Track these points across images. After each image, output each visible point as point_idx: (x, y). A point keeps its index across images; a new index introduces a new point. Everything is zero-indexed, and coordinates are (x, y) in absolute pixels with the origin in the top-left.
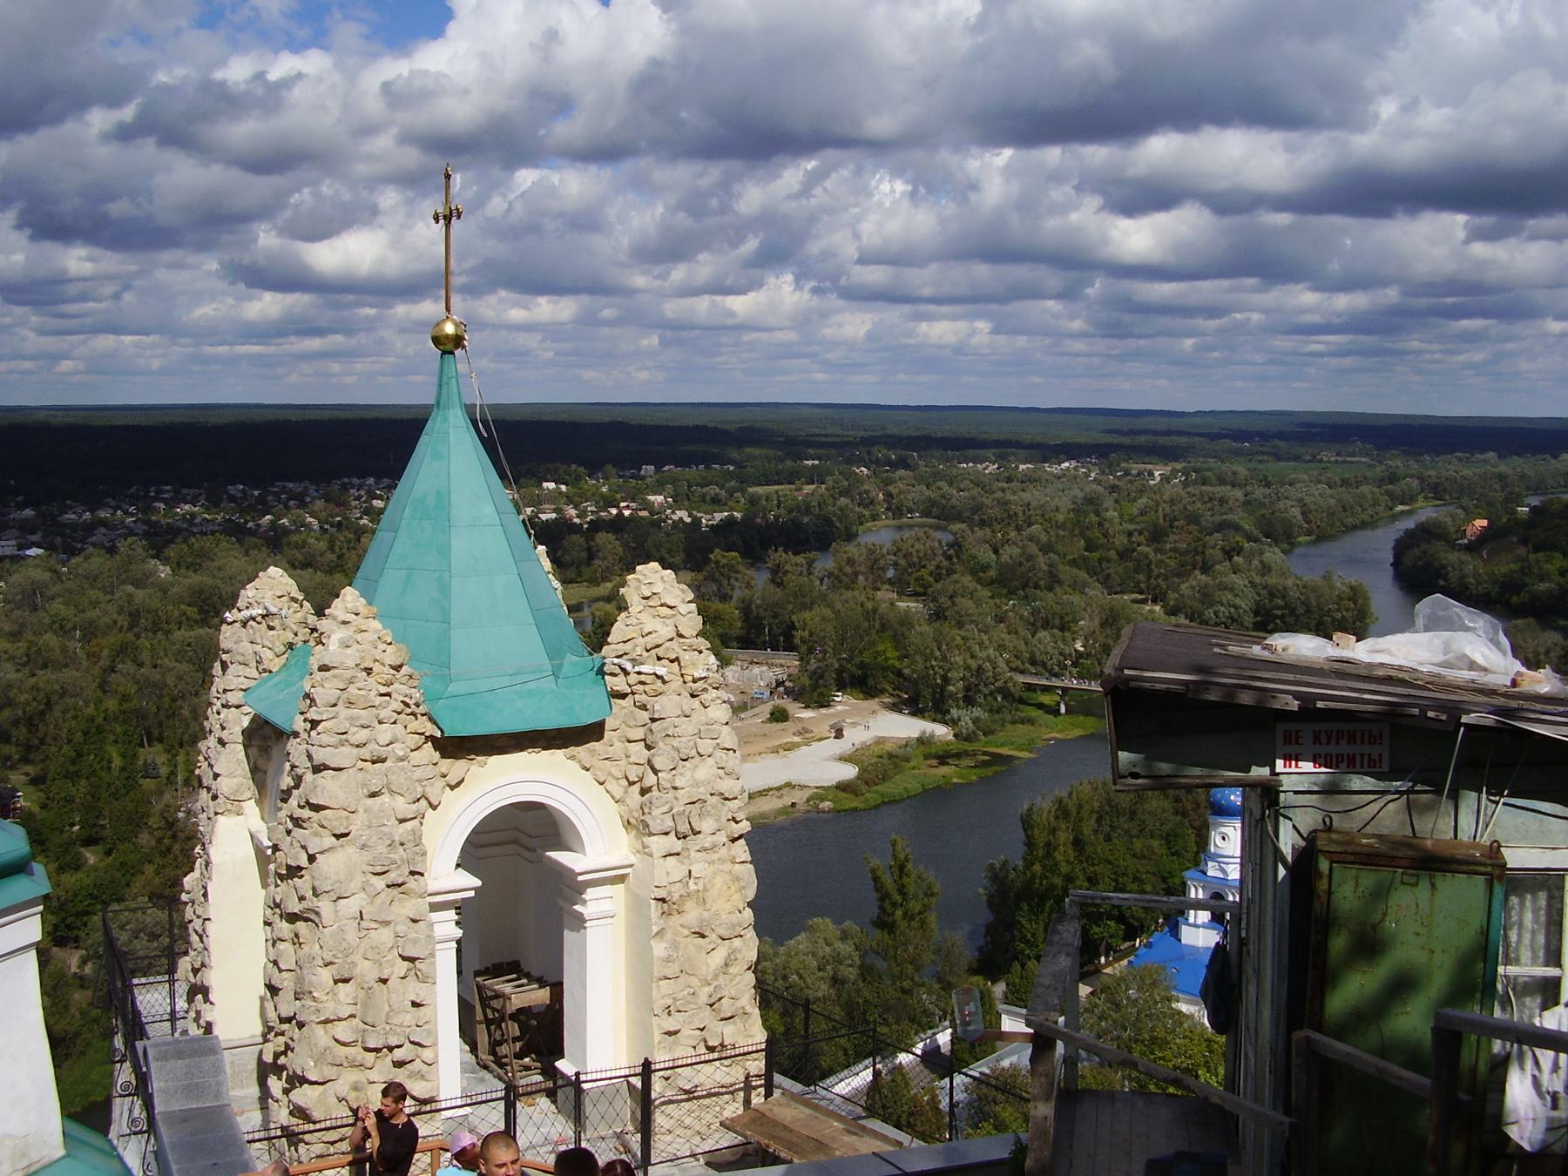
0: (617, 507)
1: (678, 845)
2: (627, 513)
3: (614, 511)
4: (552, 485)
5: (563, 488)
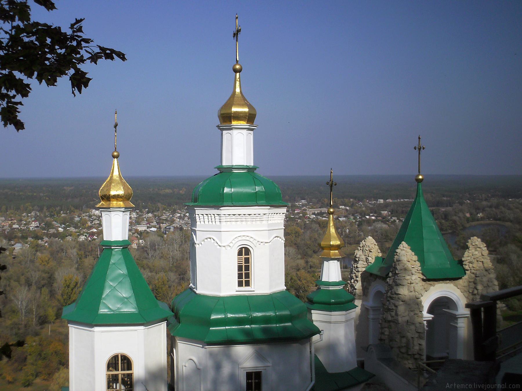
0: (369, 215)
2: (24, 214)
3: (368, 217)
4: (343, 207)
5: (348, 208)
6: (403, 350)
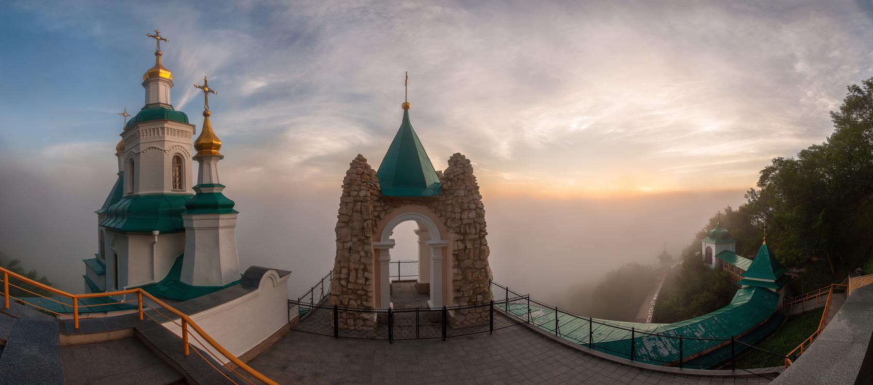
1: (462, 238)
6: (343, 283)
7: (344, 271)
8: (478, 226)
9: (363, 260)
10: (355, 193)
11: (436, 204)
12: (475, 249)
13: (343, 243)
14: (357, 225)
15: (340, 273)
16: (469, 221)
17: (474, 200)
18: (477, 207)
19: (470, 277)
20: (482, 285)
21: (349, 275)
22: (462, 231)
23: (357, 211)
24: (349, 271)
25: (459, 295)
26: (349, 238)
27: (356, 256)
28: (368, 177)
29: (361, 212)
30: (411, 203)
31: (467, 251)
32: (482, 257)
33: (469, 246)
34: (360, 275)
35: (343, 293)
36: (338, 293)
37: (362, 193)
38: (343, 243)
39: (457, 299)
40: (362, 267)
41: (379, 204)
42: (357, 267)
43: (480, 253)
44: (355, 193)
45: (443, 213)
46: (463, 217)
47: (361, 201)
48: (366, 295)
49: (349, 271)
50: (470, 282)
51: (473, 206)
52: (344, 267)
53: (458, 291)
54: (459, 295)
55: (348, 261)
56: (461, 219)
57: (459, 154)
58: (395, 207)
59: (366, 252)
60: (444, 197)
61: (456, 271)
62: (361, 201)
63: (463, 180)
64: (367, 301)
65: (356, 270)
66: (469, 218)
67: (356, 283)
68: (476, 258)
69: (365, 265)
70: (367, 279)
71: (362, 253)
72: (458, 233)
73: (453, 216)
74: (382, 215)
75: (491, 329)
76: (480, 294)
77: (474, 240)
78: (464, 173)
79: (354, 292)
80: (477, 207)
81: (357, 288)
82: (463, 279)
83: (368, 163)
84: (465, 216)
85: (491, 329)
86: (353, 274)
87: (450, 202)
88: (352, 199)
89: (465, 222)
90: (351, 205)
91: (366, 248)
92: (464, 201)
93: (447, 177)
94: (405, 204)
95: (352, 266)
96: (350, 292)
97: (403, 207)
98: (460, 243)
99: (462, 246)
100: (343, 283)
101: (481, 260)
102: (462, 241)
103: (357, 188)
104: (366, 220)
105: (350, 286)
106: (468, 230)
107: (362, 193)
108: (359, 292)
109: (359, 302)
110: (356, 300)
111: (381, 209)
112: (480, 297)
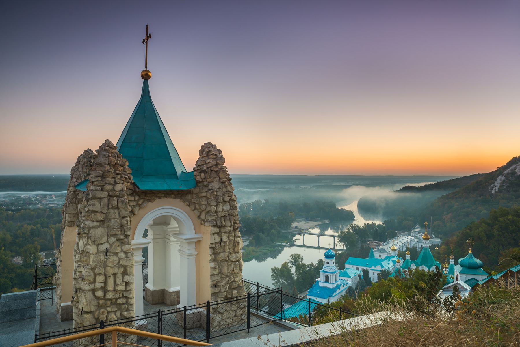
1: (217, 230)
6: (100, 294)
7: (100, 279)
8: (233, 219)
9: (123, 262)
10: (110, 187)
11: (189, 197)
12: (230, 241)
13: (98, 245)
14: (114, 223)
15: (95, 282)
16: (223, 214)
17: (228, 192)
18: (231, 200)
19: (225, 270)
20: (237, 279)
21: (105, 282)
22: (219, 224)
23: (113, 208)
24: (106, 277)
25: (217, 290)
26: (105, 239)
27: (114, 259)
28: (122, 168)
29: (118, 208)
30: (165, 197)
31: (223, 244)
32: (236, 249)
33: (225, 238)
34: (119, 281)
35: (99, 306)
36: (93, 309)
37: (119, 187)
38: (98, 245)
39: (214, 294)
40: (122, 270)
41: (133, 198)
42: (116, 270)
43: (235, 245)
44: (110, 187)
45: (197, 206)
46: (219, 210)
47: (116, 196)
48: (127, 303)
49: (106, 277)
50: (227, 276)
51: (227, 199)
52: (100, 274)
53: (215, 286)
54: (217, 290)
55: (105, 266)
56: (216, 212)
57: (210, 143)
58: (149, 201)
59: (126, 253)
60: (197, 190)
61: (213, 264)
62: (116, 196)
63: (216, 172)
64: (127, 310)
65: (115, 275)
66: (223, 211)
67: (115, 290)
68: (231, 250)
69: (125, 267)
70: (127, 284)
71: (122, 255)
72: (214, 226)
73: (208, 209)
74: (136, 210)
75: (249, 327)
76: (235, 288)
77: (229, 232)
78: (216, 165)
79: (114, 302)
80: (231, 200)
81: (117, 296)
82: (220, 272)
83: (280, 255)
84: (220, 209)
85: (249, 327)
86: (111, 281)
87: (204, 194)
88: (107, 193)
89: (220, 214)
90: (106, 201)
91: (126, 248)
92: (218, 193)
93: (199, 168)
94: (160, 198)
95: (110, 271)
96: (108, 303)
97: (157, 201)
98: (216, 235)
99: (218, 239)
100: (100, 294)
101: (235, 252)
102: (218, 233)
103: (111, 181)
104: (124, 217)
105: (109, 296)
106: (224, 223)
107: (119, 187)
108: (119, 301)
109: (118, 314)
110: (115, 312)
111: (135, 203)
112: (235, 292)
